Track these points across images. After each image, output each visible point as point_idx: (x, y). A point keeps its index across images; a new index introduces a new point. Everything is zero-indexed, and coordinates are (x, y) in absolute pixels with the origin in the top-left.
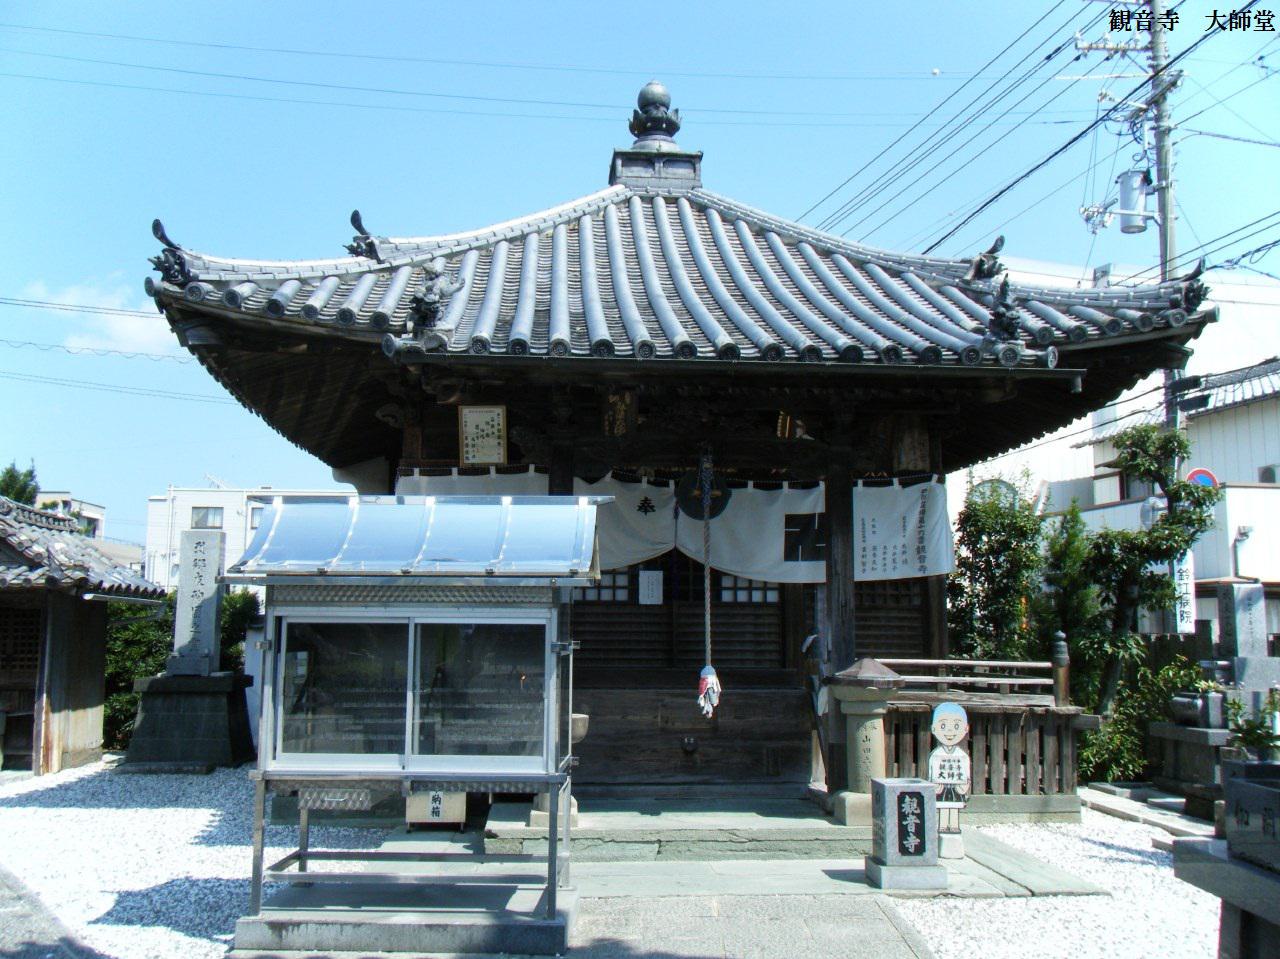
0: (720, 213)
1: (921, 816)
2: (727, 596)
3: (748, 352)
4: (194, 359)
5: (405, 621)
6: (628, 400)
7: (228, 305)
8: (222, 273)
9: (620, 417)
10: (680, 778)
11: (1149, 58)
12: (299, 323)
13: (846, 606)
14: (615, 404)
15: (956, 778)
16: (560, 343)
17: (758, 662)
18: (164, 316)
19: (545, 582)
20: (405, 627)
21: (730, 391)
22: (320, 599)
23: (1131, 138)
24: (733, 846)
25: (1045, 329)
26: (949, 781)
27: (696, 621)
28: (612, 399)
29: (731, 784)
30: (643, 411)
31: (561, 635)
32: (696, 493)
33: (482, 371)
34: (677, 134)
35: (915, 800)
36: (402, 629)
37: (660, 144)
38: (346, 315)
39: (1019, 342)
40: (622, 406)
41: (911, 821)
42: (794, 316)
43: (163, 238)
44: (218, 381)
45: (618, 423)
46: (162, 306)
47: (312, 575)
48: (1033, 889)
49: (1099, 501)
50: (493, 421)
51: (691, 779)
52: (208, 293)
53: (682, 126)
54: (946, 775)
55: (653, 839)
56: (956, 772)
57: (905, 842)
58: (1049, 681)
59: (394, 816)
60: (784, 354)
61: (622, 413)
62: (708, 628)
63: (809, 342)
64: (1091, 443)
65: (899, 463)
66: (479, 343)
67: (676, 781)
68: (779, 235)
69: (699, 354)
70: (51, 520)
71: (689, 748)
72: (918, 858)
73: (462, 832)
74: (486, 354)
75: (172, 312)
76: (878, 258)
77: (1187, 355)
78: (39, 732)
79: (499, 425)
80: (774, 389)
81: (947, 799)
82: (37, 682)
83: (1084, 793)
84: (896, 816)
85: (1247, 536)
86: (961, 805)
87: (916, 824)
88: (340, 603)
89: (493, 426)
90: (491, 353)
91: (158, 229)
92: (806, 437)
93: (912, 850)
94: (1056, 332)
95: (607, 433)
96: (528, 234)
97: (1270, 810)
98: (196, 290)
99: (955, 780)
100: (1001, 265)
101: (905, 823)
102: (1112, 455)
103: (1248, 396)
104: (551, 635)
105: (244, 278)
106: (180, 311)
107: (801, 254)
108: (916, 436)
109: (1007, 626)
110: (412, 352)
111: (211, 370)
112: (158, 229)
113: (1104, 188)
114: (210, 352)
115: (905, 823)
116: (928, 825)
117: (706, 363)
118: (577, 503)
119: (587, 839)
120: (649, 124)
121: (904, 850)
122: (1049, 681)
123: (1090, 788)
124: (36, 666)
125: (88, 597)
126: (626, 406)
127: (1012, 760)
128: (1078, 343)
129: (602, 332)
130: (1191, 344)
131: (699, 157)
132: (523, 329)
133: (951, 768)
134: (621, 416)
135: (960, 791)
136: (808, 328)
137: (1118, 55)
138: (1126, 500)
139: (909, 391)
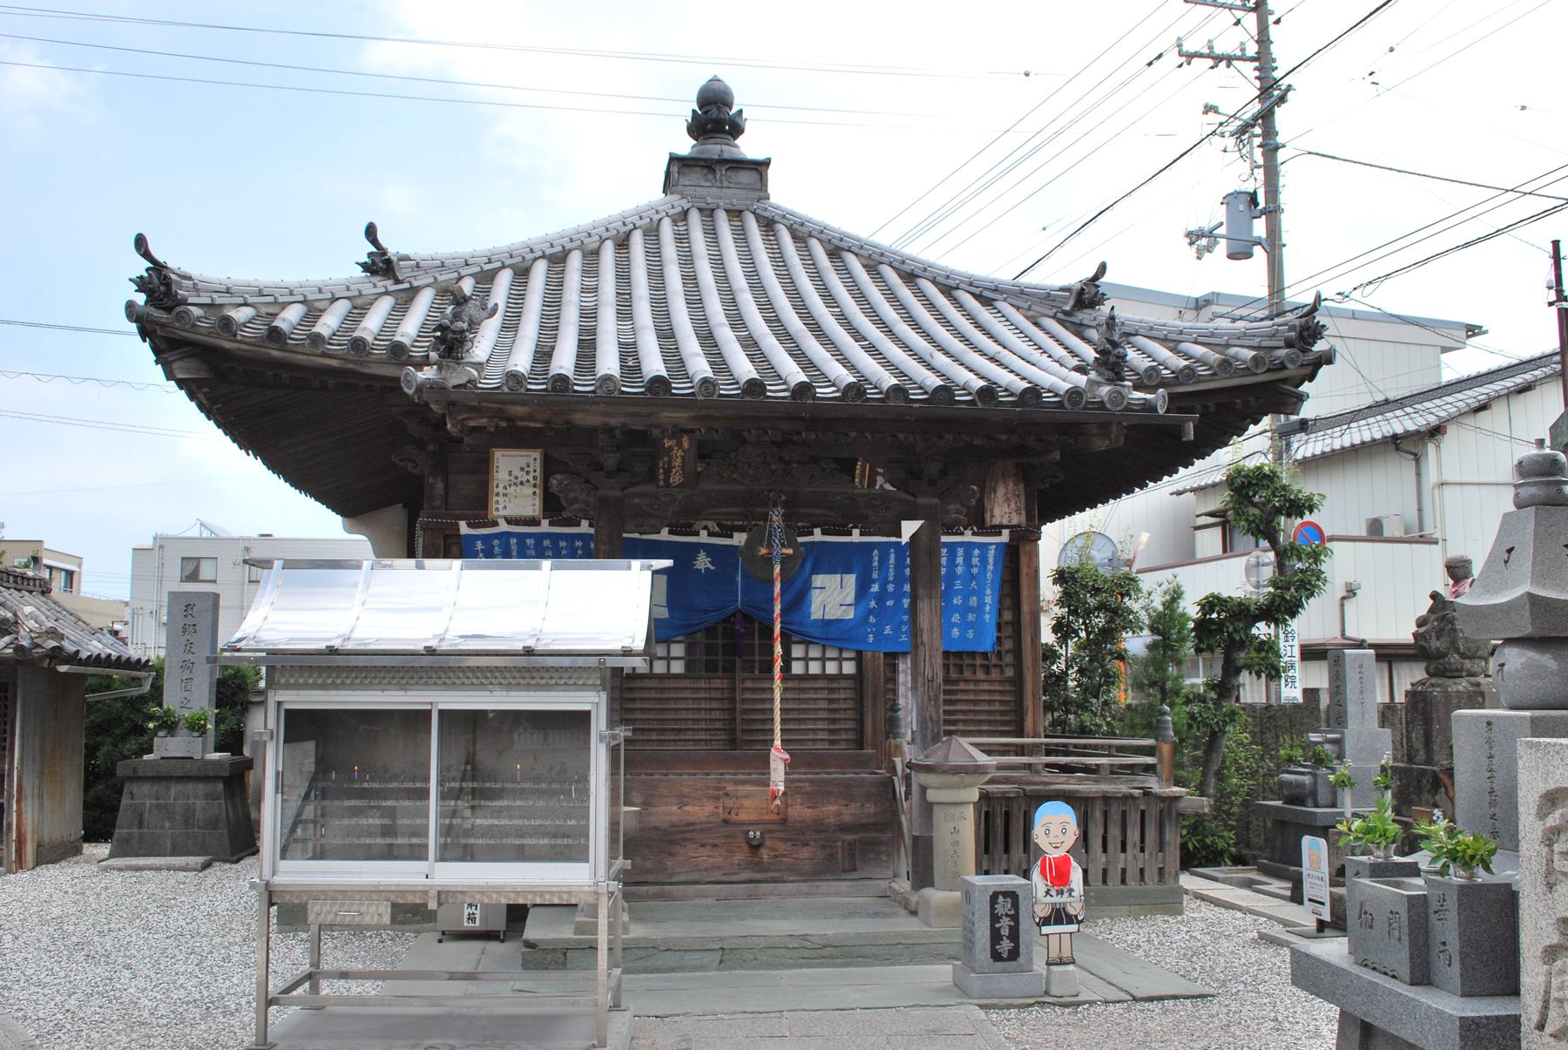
0: (790, 228)
1: (1015, 918)
2: (797, 668)
3: (824, 391)
4: (182, 395)
5: (429, 707)
6: (686, 445)
7: (221, 333)
8: (215, 296)
9: (677, 464)
10: (746, 875)
11: (1256, 69)
12: (303, 354)
13: (932, 681)
14: (671, 448)
15: (1066, 895)
16: (608, 378)
17: (832, 742)
18: (147, 344)
19: (593, 662)
20: (430, 711)
21: (804, 434)
22: (329, 681)
23: (1237, 155)
24: (806, 953)
25: (1152, 368)
27: (764, 696)
28: (668, 443)
29: (803, 881)
30: (702, 456)
31: (612, 724)
32: (763, 551)
33: (520, 410)
34: (741, 137)
35: (1009, 900)
36: (425, 715)
37: (714, 149)
38: (358, 344)
39: (1126, 383)
40: (678, 453)
41: (1005, 925)
42: (872, 350)
43: (147, 255)
44: (210, 419)
45: (674, 471)
46: (144, 333)
47: (319, 653)
49: (1199, 556)
50: (528, 466)
51: (758, 876)
52: (199, 319)
53: (748, 127)
55: (716, 947)
57: (997, 947)
58: (1150, 760)
59: (418, 922)
60: (865, 393)
61: (679, 460)
62: (777, 705)
63: (894, 381)
64: (1192, 490)
65: (992, 516)
66: (514, 377)
67: (741, 879)
68: (857, 255)
69: (768, 394)
70: (19, 580)
71: (755, 843)
72: (1012, 963)
73: (502, 941)
74: (523, 391)
75: (156, 340)
76: (971, 284)
77: (1301, 398)
78: (10, 825)
79: (535, 471)
80: (853, 434)
81: (1056, 923)
83: (1187, 881)
84: (988, 918)
85: (1355, 594)
86: (1073, 928)
88: (352, 687)
89: (528, 473)
90: (528, 390)
91: (141, 243)
92: (888, 487)
93: (1005, 956)
94: (1164, 372)
95: (661, 483)
96: (570, 251)
97: (1397, 913)
98: (182, 316)
99: (1065, 898)
100: (1103, 294)
102: (1217, 502)
103: (1357, 441)
104: (599, 723)
105: (240, 301)
106: (166, 339)
107: (845, 271)
108: (1010, 487)
110: (435, 388)
111: (201, 407)
112: (141, 243)
113: (1213, 214)
114: (200, 388)
117: (778, 404)
118: (629, 568)
119: (639, 948)
120: (709, 126)
121: (996, 956)
122: (1150, 760)
123: (1192, 874)
125: (63, 669)
126: (683, 451)
127: (1110, 847)
128: (1187, 385)
129: (654, 365)
130: (1306, 387)
132: (564, 361)
134: (678, 462)
135: (1071, 911)
136: (888, 364)
137: (1223, 64)
138: (1229, 554)
139: (1004, 437)
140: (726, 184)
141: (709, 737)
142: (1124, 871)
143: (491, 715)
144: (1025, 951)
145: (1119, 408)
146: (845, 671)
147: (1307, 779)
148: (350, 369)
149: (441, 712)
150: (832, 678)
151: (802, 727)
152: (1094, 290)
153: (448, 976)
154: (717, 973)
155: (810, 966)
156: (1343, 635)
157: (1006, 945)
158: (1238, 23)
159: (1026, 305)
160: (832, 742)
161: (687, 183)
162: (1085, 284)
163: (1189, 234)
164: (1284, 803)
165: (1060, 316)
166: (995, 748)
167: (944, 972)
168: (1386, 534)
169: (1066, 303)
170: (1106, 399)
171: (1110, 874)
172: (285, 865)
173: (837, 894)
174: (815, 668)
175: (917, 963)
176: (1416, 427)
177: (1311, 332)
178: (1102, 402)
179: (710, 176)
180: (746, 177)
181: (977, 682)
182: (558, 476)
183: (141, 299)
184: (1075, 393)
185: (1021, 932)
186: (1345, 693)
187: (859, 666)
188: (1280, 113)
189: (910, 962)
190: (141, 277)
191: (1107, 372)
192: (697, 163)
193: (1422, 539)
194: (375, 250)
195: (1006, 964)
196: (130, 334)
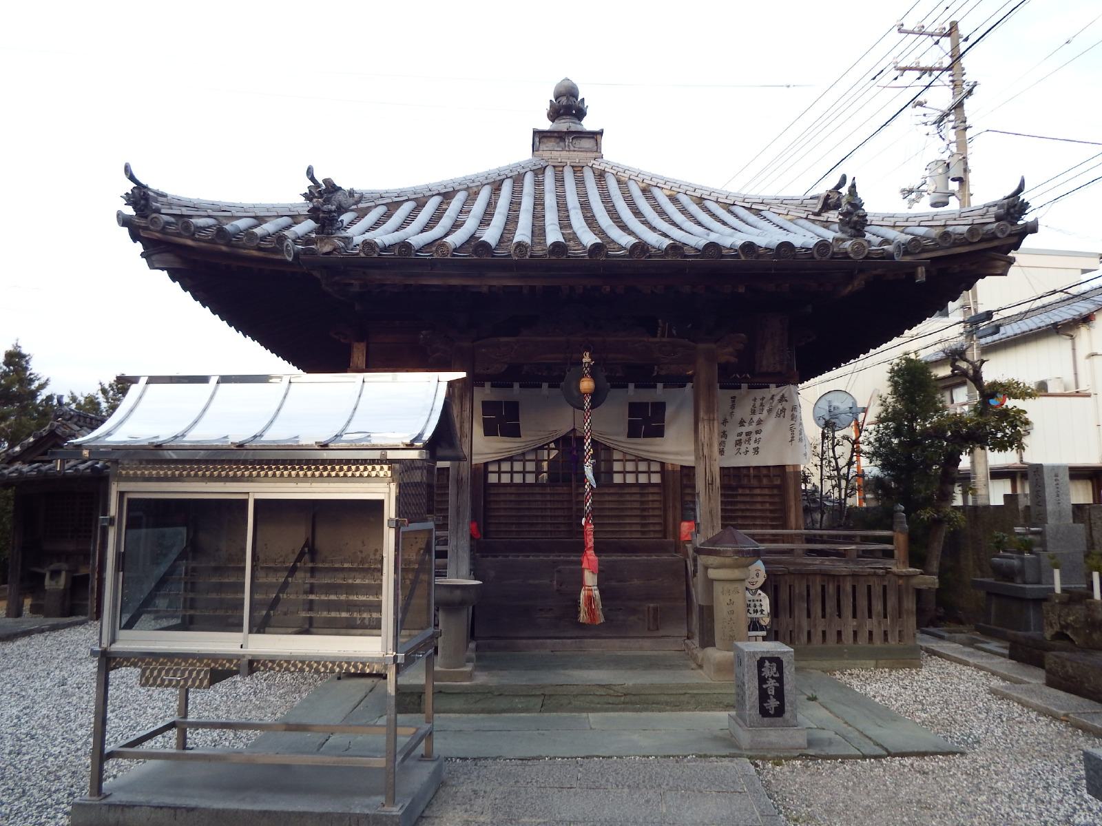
1: (780, 680)
11: (950, 75)
13: (712, 484)
17: (643, 533)
20: (245, 502)
24: (611, 700)
26: (754, 615)
34: (585, 117)
41: (771, 685)
43: (132, 178)
46: (135, 237)
48: (889, 749)
53: (588, 111)
54: (751, 611)
56: (759, 609)
57: (765, 705)
58: (889, 547)
82: (92, 548)
86: (764, 633)
87: (775, 687)
91: (127, 170)
93: (772, 712)
99: (759, 615)
101: (764, 686)
104: (390, 511)
109: (841, 502)
115: (764, 686)
116: (787, 687)
121: (764, 712)
124: (90, 537)
130: (1012, 254)
131: (601, 133)
133: (755, 606)
140: (572, 148)
141: (553, 529)
142: (871, 633)
144: (790, 708)
145: (861, 257)
146: (653, 481)
147: (1016, 562)
148: (278, 259)
149: (256, 501)
150: (643, 486)
151: (621, 522)
152: (837, 196)
153: (284, 727)
155: (614, 710)
156: (1021, 461)
157: (773, 703)
158: (937, 43)
159: (785, 212)
160: (643, 533)
161: (545, 149)
162: (830, 191)
163: (903, 191)
164: (996, 580)
165: (811, 217)
166: (767, 537)
167: (722, 718)
168: (1050, 391)
169: (815, 208)
170: (849, 250)
171: (859, 635)
172: (123, 634)
173: (641, 648)
174: (630, 479)
175: (702, 710)
176: (1071, 317)
177: (1017, 208)
178: (846, 253)
179: (562, 144)
180: (587, 143)
181: (751, 488)
182: (424, 332)
183: (130, 211)
184: (823, 245)
185: (785, 692)
186: (1045, 497)
187: (663, 478)
188: (967, 103)
189: (695, 709)
190: (127, 194)
191: (850, 230)
192: (552, 135)
193: (1077, 394)
194: (313, 184)
195: (772, 720)
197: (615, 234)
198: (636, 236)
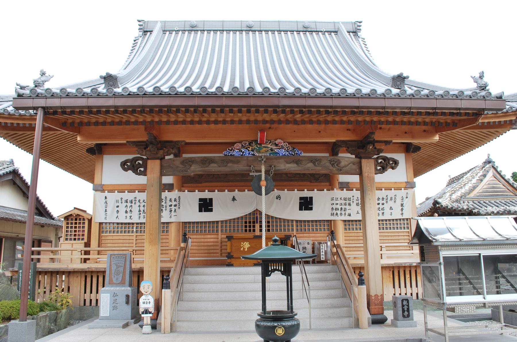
1: (408, 306)
41: (406, 308)
72: (408, 318)
93: (406, 316)
101: (404, 308)
115: (404, 308)
121: (404, 316)
131: (43, 74)
143: (481, 276)
154: (386, 126)
196: (280, 274)
197: (287, 85)
198: (312, 85)
